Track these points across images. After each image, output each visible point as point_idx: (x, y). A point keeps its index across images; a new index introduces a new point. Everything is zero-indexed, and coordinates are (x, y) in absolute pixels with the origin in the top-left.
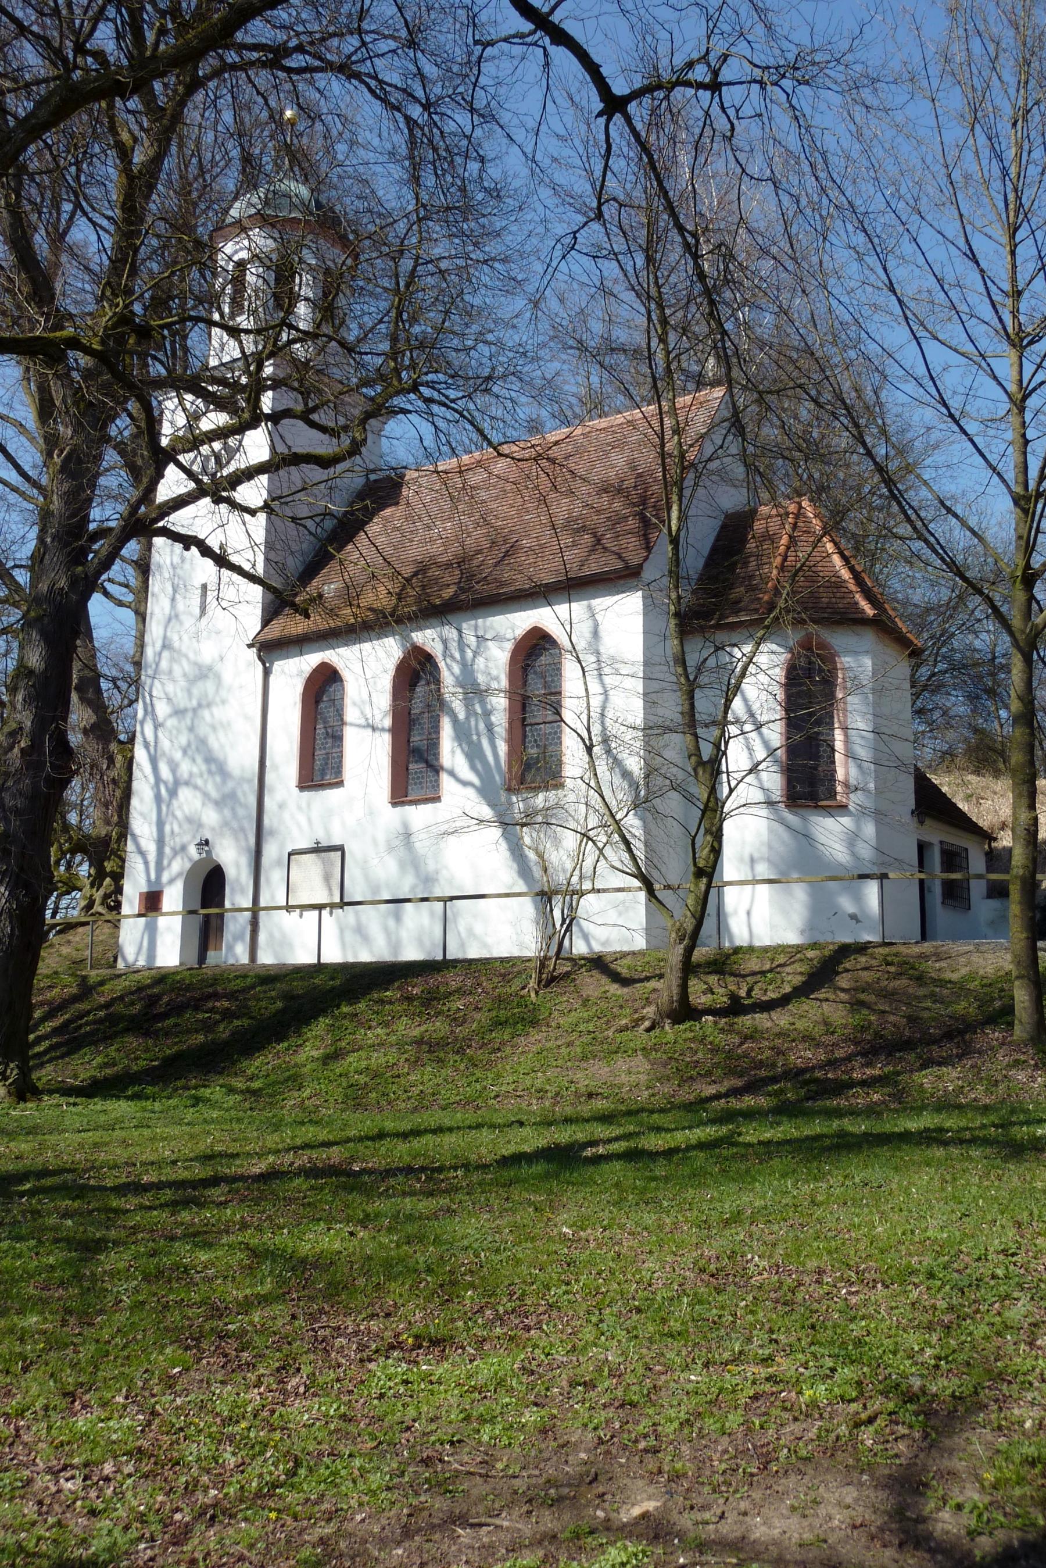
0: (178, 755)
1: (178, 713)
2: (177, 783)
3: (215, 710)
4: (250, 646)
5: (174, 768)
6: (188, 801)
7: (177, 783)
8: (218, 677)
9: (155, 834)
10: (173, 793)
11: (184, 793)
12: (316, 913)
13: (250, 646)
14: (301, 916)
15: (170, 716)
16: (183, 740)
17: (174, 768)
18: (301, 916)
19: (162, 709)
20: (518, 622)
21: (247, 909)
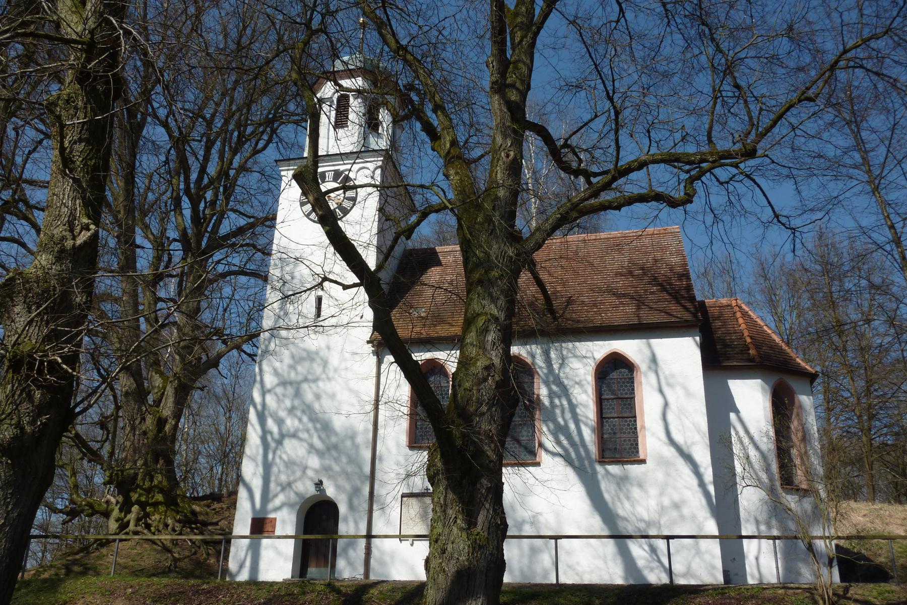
0: (282, 414)
1: (284, 383)
2: (283, 436)
3: (321, 384)
4: (368, 342)
5: (280, 422)
6: (293, 449)
7: (283, 436)
8: (325, 363)
9: (572, 397)
10: (279, 442)
11: (289, 444)
12: (553, 541)
13: (368, 342)
14: (412, 545)
15: (278, 385)
16: (288, 403)
17: (280, 422)
18: (412, 545)
19: (270, 380)
20: (600, 349)
21: (774, 543)
